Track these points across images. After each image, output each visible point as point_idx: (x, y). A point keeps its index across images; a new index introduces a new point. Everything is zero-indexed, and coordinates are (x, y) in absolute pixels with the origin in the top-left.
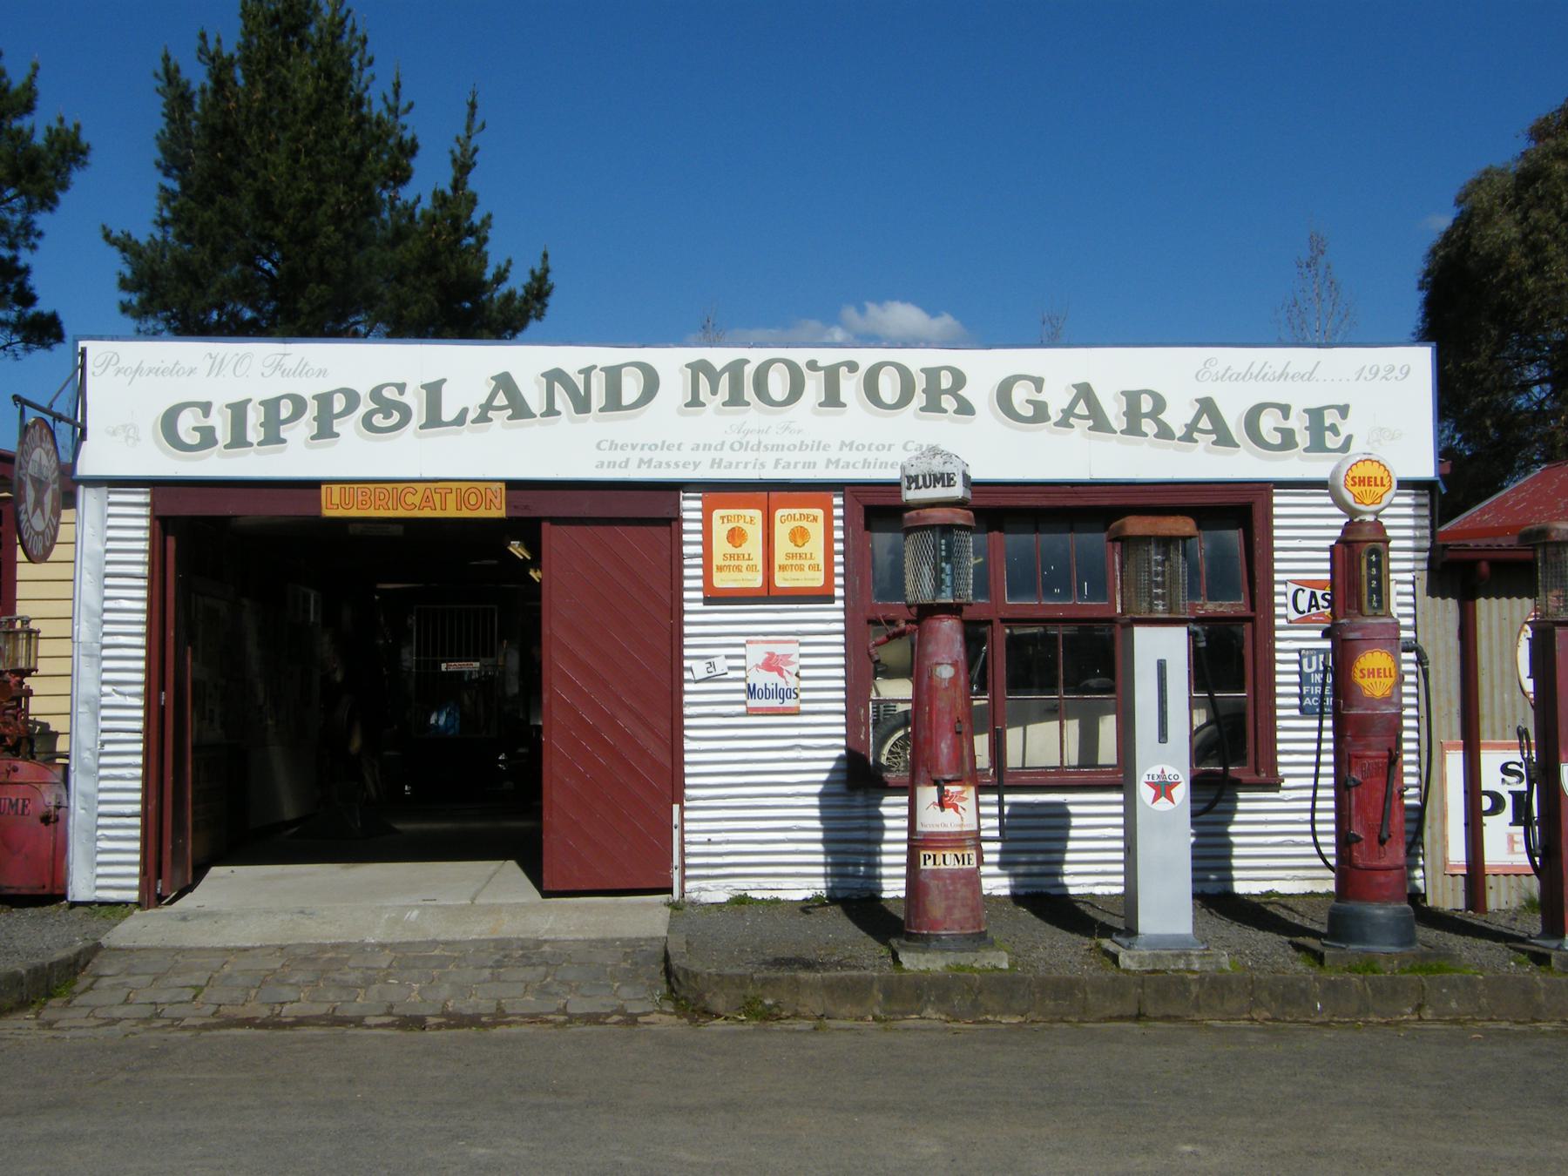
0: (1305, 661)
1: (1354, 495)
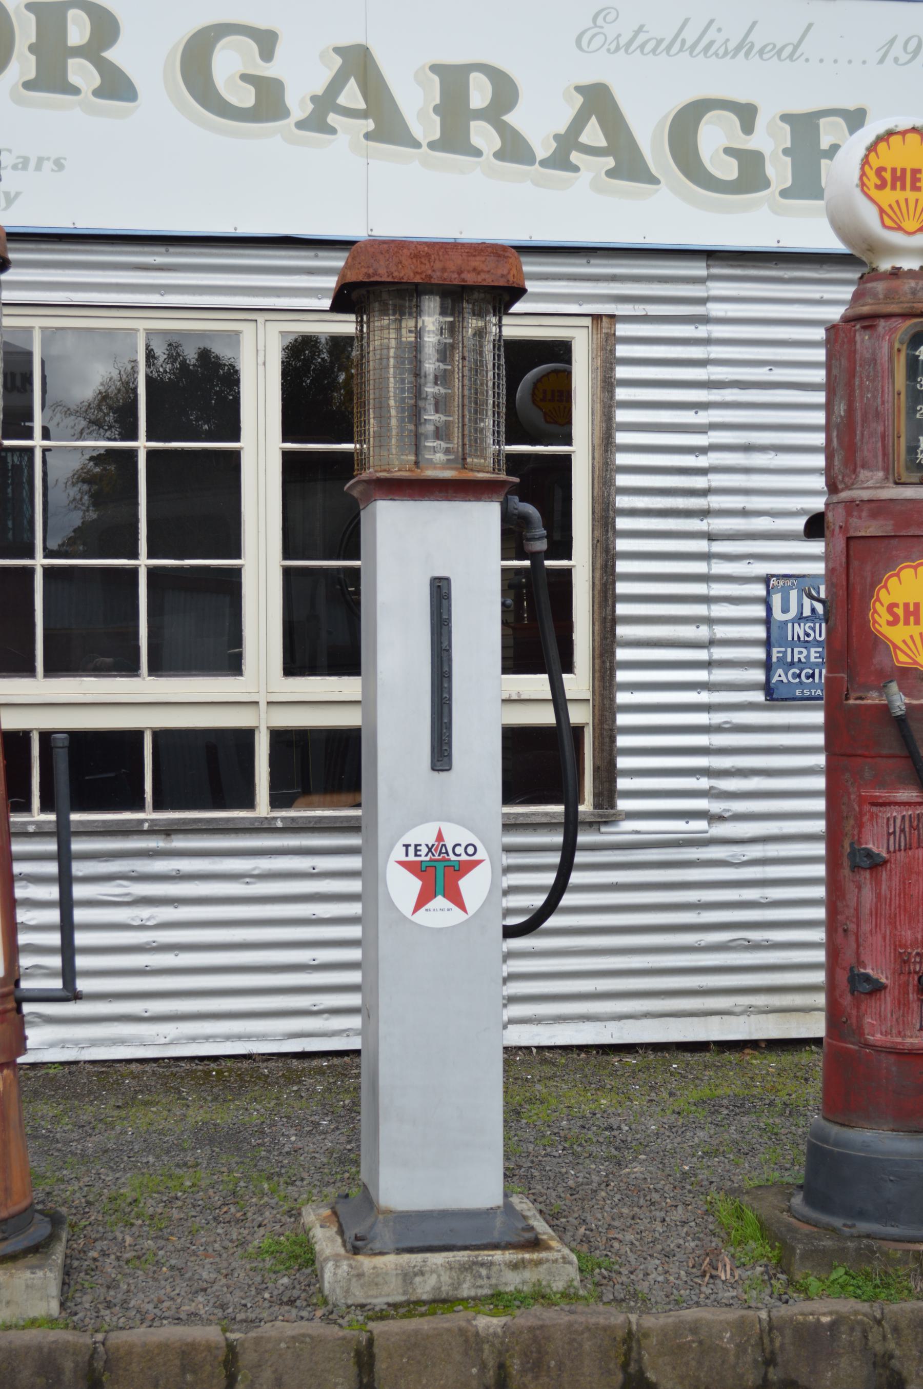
0: (776, 600)
1: (882, 211)
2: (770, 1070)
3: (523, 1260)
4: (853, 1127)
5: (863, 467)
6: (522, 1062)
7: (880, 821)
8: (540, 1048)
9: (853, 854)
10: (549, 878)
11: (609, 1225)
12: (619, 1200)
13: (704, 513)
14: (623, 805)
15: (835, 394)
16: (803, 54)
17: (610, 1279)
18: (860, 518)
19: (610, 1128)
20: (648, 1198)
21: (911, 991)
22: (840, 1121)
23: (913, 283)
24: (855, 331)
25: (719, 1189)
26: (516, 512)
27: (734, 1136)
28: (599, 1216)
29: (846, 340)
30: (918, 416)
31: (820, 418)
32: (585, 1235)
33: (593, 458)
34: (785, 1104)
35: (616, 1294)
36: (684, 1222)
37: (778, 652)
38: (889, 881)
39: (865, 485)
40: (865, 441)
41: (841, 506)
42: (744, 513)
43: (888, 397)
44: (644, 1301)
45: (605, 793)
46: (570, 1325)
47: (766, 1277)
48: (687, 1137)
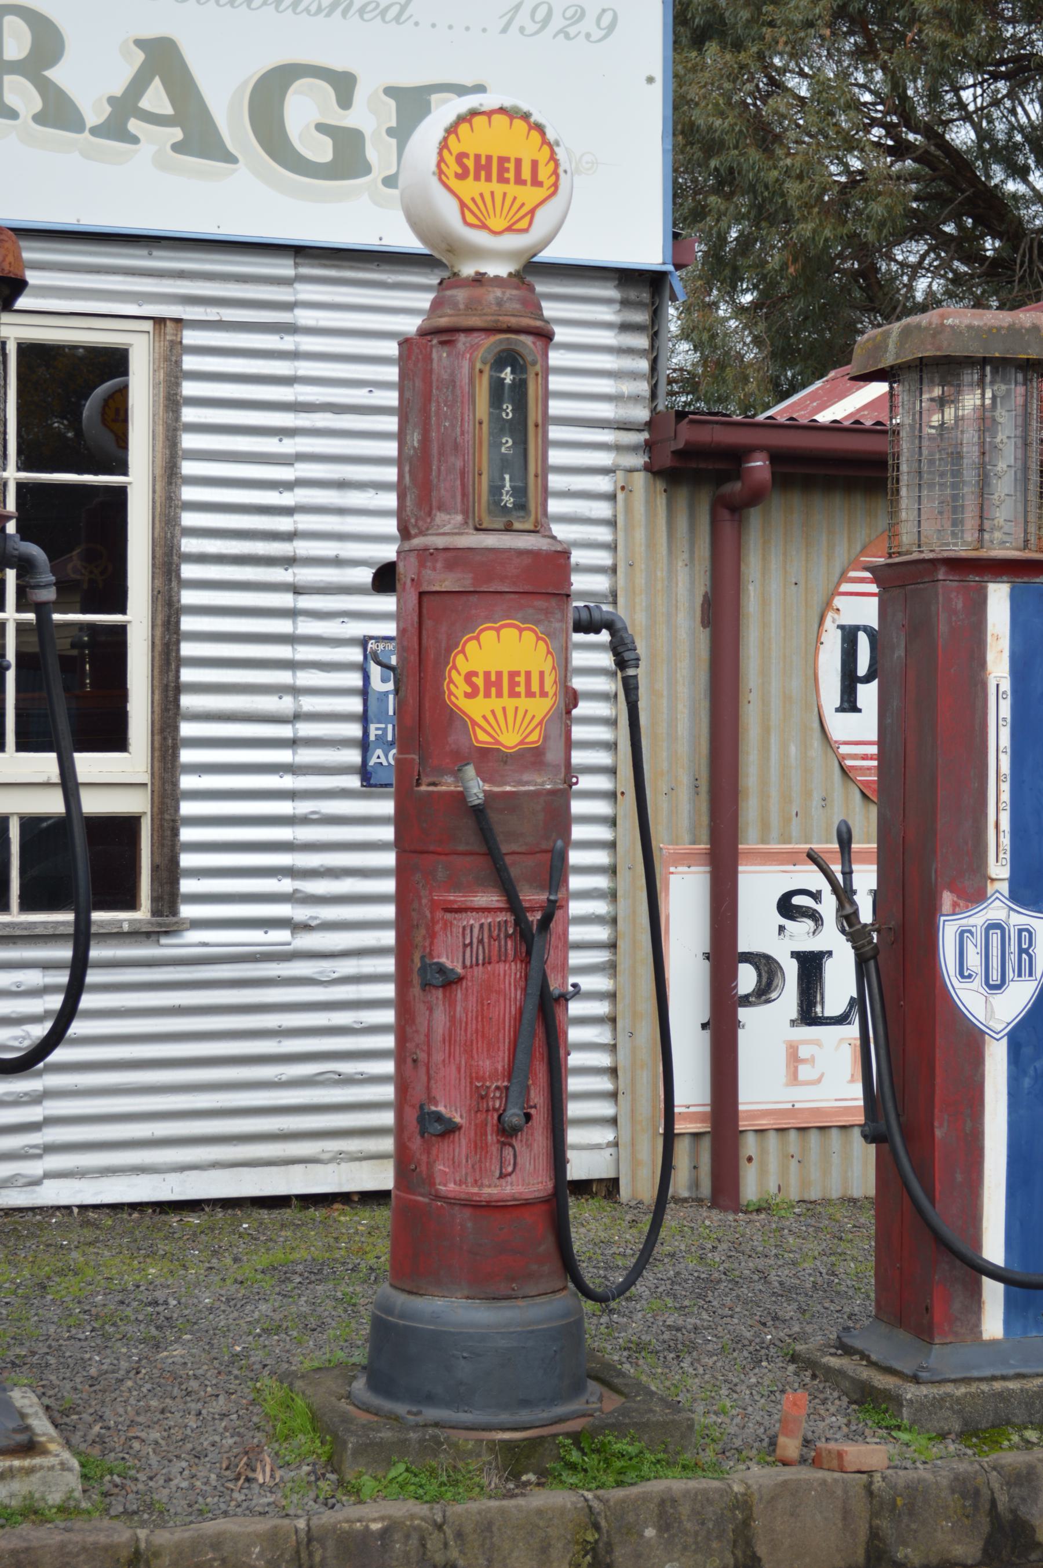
1: (463, 205)
2: (360, 1228)
3: (11, 1469)
4: (422, 1295)
5: (439, 509)
6: (59, 1224)
7: (454, 930)
8: (83, 1208)
9: (423, 969)
10: (55, 1002)
11: (132, 1421)
12: (149, 1391)
13: (289, 561)
14: (187, 911)
15: (407, 421)
16: (411, 16)
17: (123, 1487)
18: (434, 569)
19: (155, 1303)
20: (184, 1387)
21: (489, 1132)
22: (408, 1288)
23: (498, 293)
24: (432, 346)
25: (272, 1373)
26: (16, 553)
27: (303, 1309)
28: (121, 1410)
29: (420, 357)
30: (503, 450)
31: (391, 449)
32: (99, 1435)
33: (154, 492)
34: (371, 1268)
35: (128, 1505)
36: (224, 1415)
37: (377, 729)
38: (465, 1001)
39: (442, 531)
40: (441, 478)
41: (414, 554)
42: (337, 562)
43: (468, 427)
44: (161, 1512)
45: (166, 897)
46: (62, 1546)
47: (313, 1478)
48: (246, 1312)
